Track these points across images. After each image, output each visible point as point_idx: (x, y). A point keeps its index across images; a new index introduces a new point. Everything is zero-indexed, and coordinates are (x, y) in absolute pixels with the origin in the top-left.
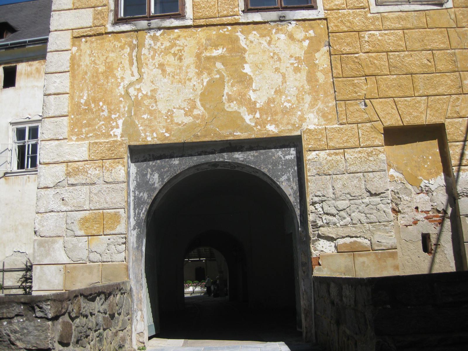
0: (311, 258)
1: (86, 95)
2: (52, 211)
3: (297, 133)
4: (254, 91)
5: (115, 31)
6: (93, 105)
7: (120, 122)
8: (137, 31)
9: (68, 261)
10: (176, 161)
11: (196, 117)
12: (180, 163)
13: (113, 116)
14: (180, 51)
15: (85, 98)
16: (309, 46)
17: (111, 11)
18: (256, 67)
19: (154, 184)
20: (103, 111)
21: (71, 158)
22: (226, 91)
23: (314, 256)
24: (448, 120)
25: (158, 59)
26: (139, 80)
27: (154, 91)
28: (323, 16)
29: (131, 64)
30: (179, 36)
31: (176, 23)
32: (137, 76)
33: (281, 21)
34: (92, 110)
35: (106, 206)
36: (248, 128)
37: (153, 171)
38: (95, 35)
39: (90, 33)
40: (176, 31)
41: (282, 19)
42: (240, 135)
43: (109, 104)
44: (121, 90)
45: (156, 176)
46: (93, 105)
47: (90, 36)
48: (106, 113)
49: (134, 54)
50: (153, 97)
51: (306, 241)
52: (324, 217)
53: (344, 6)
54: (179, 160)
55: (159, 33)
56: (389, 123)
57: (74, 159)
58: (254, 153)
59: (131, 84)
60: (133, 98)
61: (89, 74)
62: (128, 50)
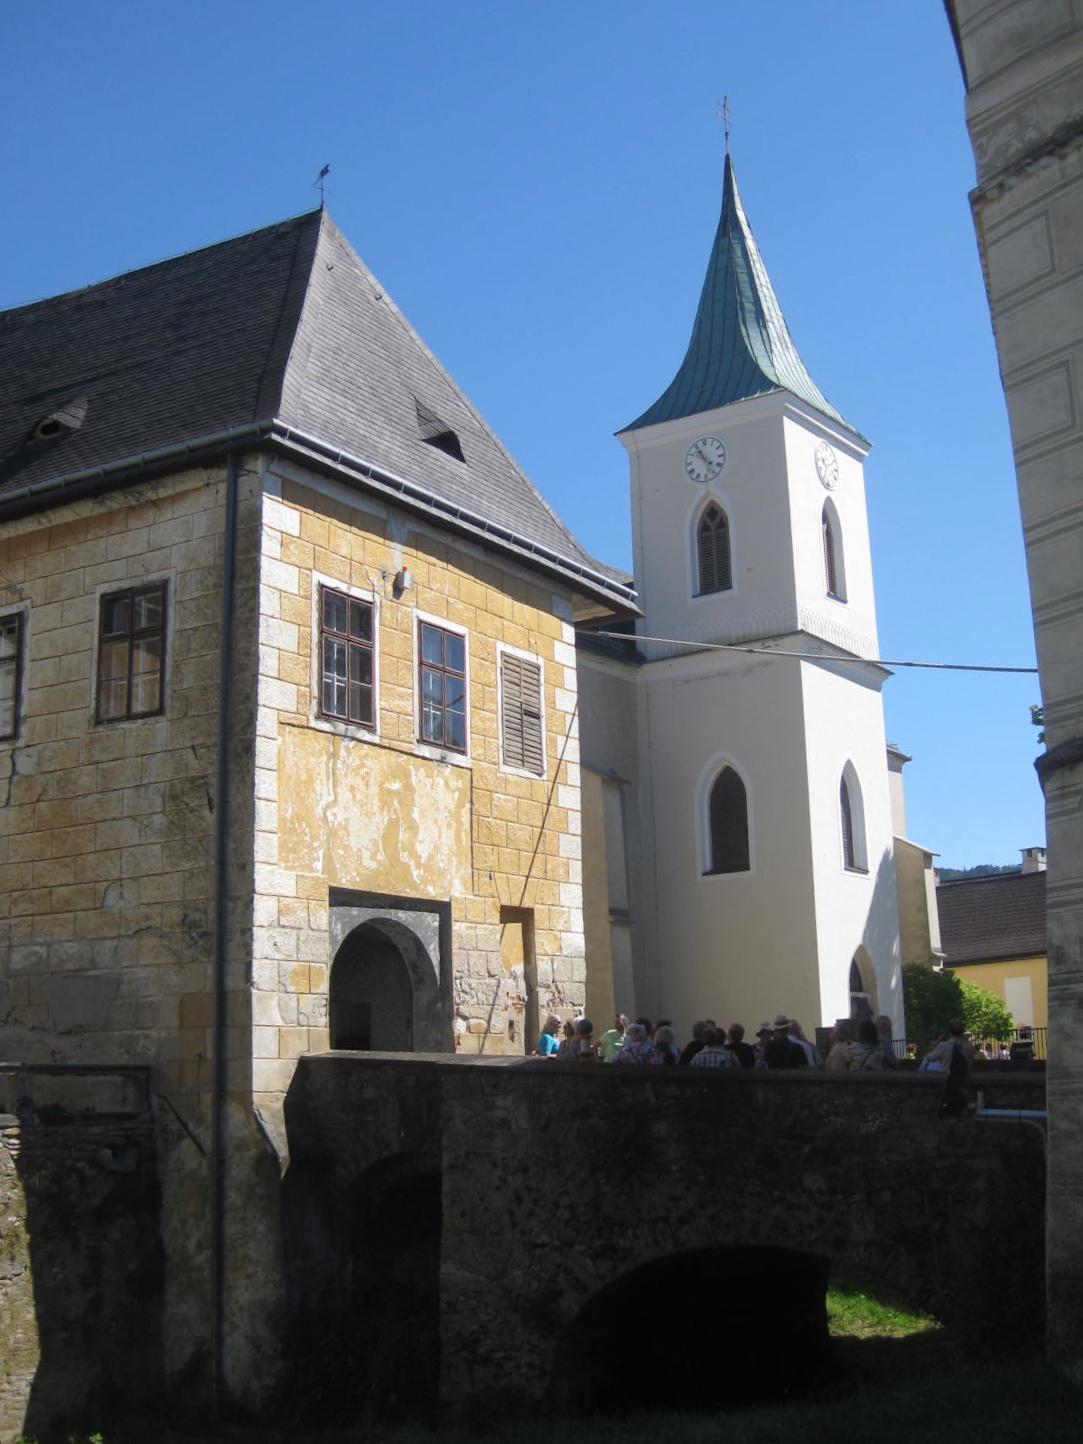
0: (453, 1037)
1: (290, 808)
2: (266, 958)
3: (447, 900)
4: (420, 842)
5: (317, 727)
6: (297, 824)
7: (321, 853)
8: (334, 734)
9: (283, 1024)
10: (355, 911)
11: (379, 863)
12: (358, 915)
13: (315, 845)
14: (368, 774)
15: (290, 812)
16: (459, 796)
17: (315, 697)
18: (423, 813)
19: (337, 936)
20: (306, 835)
21: (282, 892)
22: (400, 837)
23: (455, 1035)
24: (537, 906)
25: (350, 779)
26: (335, 801)
27: (346, 820)
28: (469, 766)
29: (328, 778)
30: (367, 755)
31: (364, 735)
32: (328, 813)
33: (442, 762)
34: (295, 830)
35: (314, 958)
36: (414, 886)
37: (337, 920)
38: (298, 726)
39: (296, 722)
40: (366, 746)
41: (442, 761)
42: (410, 893)
43: (310, 827)
44: (319, 811)
45: (339, 926)
46: (297, 824)
47: (293, 726)
48: (307, 838)
49: (331, 765)
50: (346, 828)
51: (896, 1310)
52: (462, 994)
53: (482, 758)
54: (359, 911)
55: (352, 744)
56: (506, 902)
57: (137, 686)
58: (411, 914)
59: (328, 807)
60: (331, 824)
61: (293, 780)
62: (324, 758)
